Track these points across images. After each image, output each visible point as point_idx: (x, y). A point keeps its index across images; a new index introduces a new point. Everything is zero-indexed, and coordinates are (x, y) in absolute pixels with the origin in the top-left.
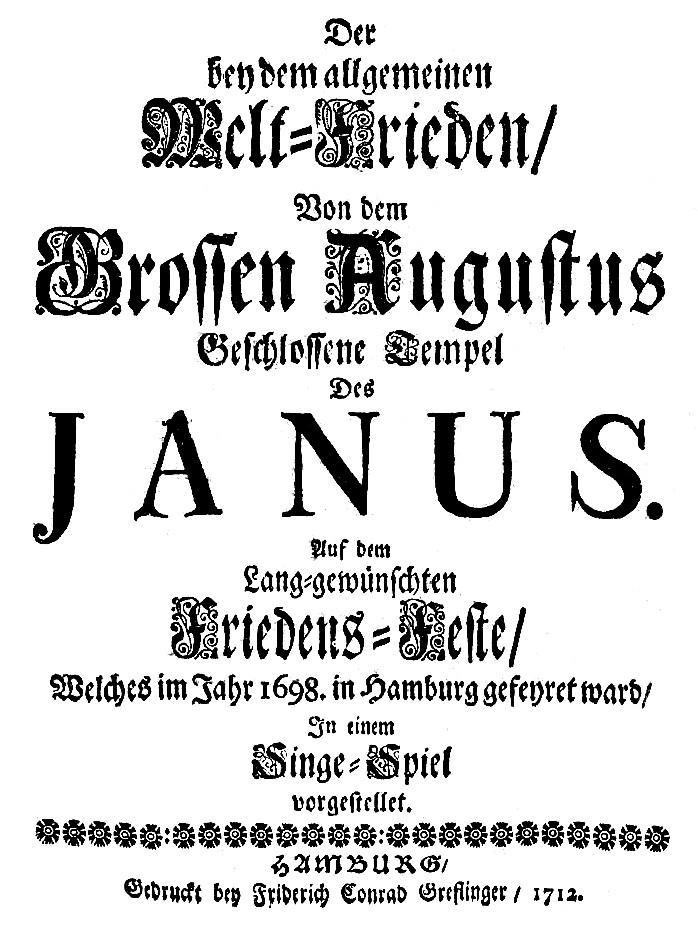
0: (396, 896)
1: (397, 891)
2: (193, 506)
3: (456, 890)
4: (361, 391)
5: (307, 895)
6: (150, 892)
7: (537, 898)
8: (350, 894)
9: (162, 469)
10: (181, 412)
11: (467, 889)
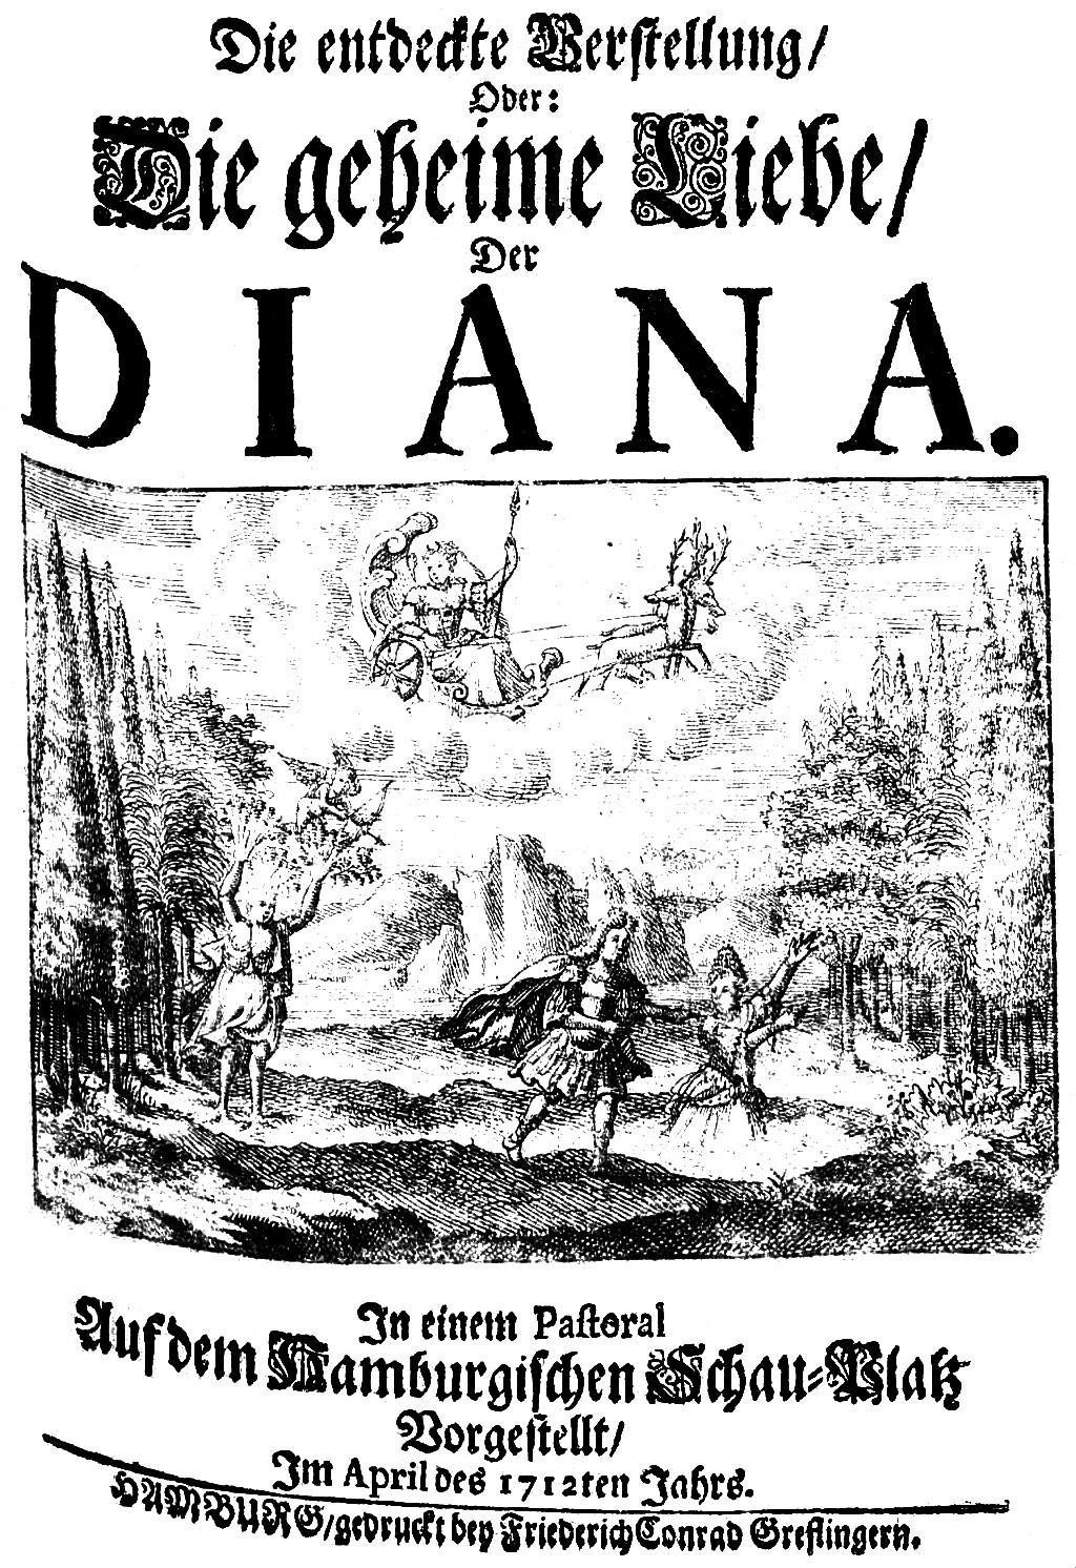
0: (725, 1538)
1: (726, 1529)
2: (503, 436)
6: (556, 1536)
8: (651, 1535)
9: (890, 375)
10: (924, 286)
11: (829, 1529)
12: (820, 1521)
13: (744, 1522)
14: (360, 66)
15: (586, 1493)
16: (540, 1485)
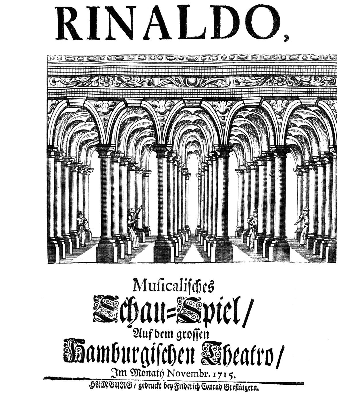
3: (236, 386)
4: (207, 289)
5: (192, 387)
7: (215, 376)
9: (152, 23)
11: (240, 386)
12: (238, 384)
13: (223, 384)
14: (156, 305)
15: (118, 382)
16: (223, 375)
